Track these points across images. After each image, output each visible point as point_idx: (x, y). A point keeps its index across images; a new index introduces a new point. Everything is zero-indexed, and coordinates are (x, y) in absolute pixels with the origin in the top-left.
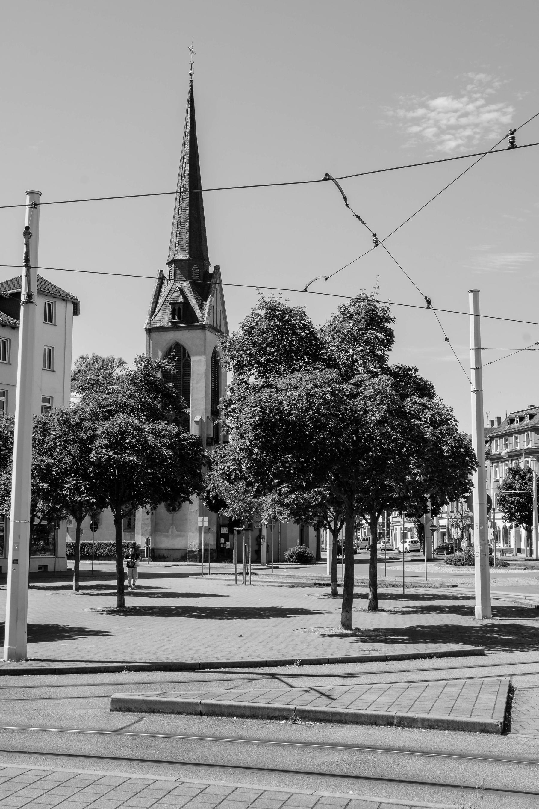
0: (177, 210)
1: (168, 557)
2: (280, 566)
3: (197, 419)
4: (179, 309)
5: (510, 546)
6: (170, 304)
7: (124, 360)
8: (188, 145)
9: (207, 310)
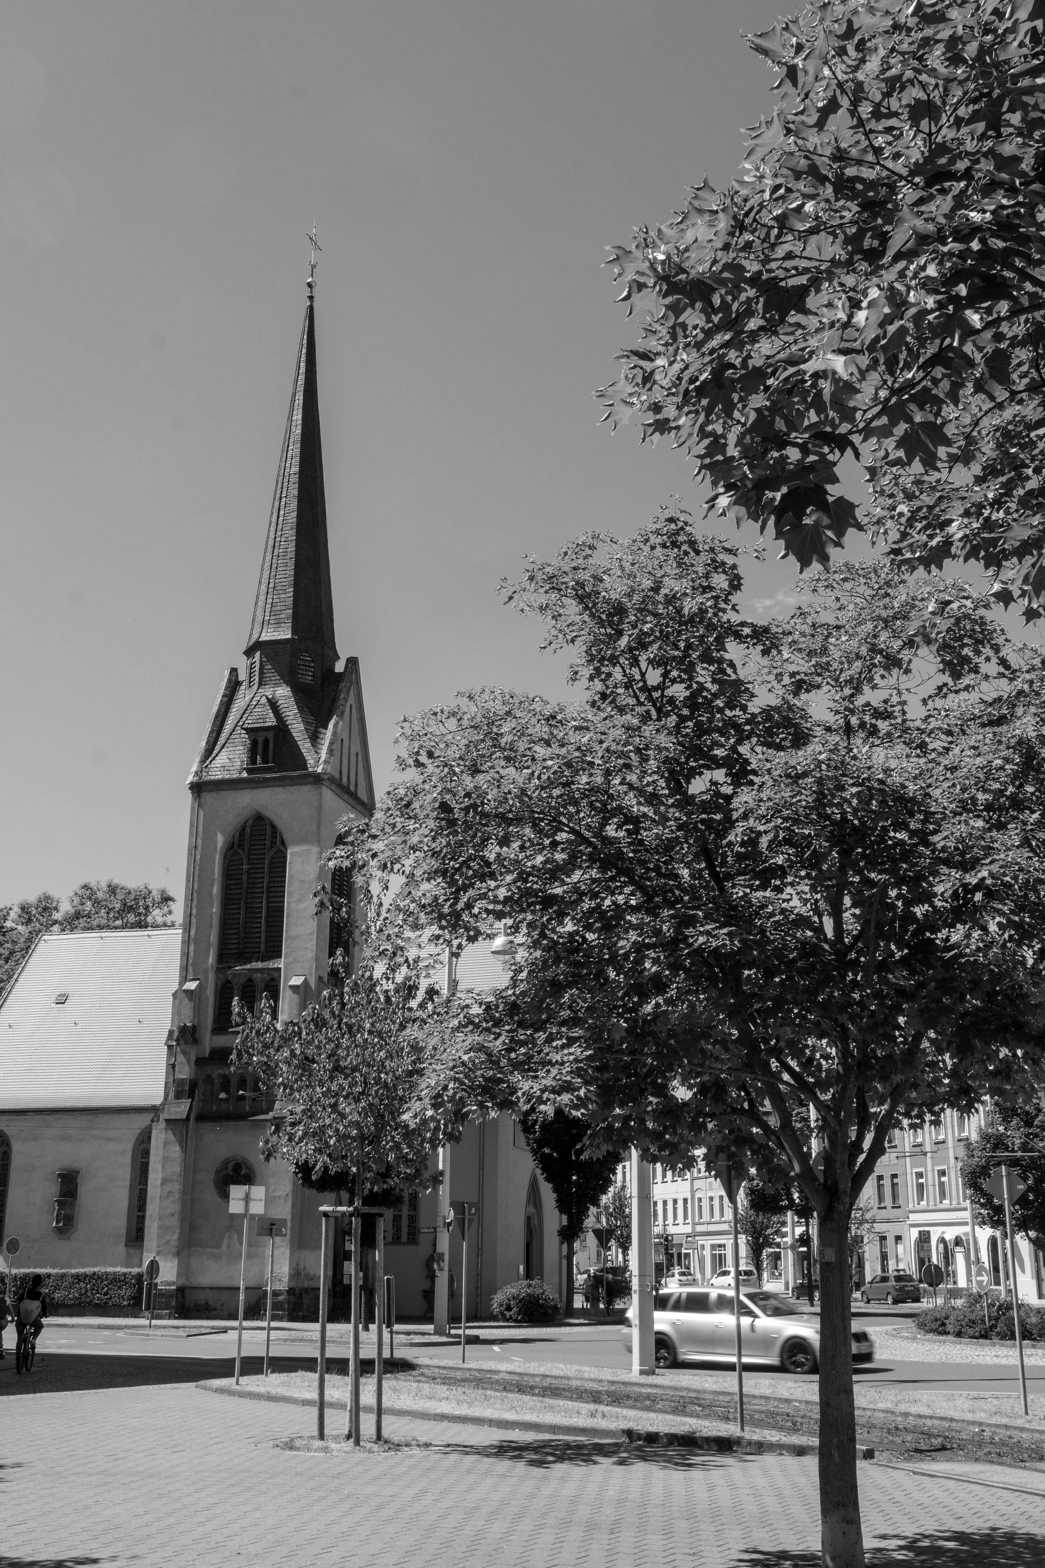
0: (271, 543)
1: (215, 1309)
2: (483, 1333)
3: (296, 981)
4: (266, 742)
5: (955, 1283)
6: (249, 731)
7: (171, 894)
8: (300, 416)
9: (327, 743)
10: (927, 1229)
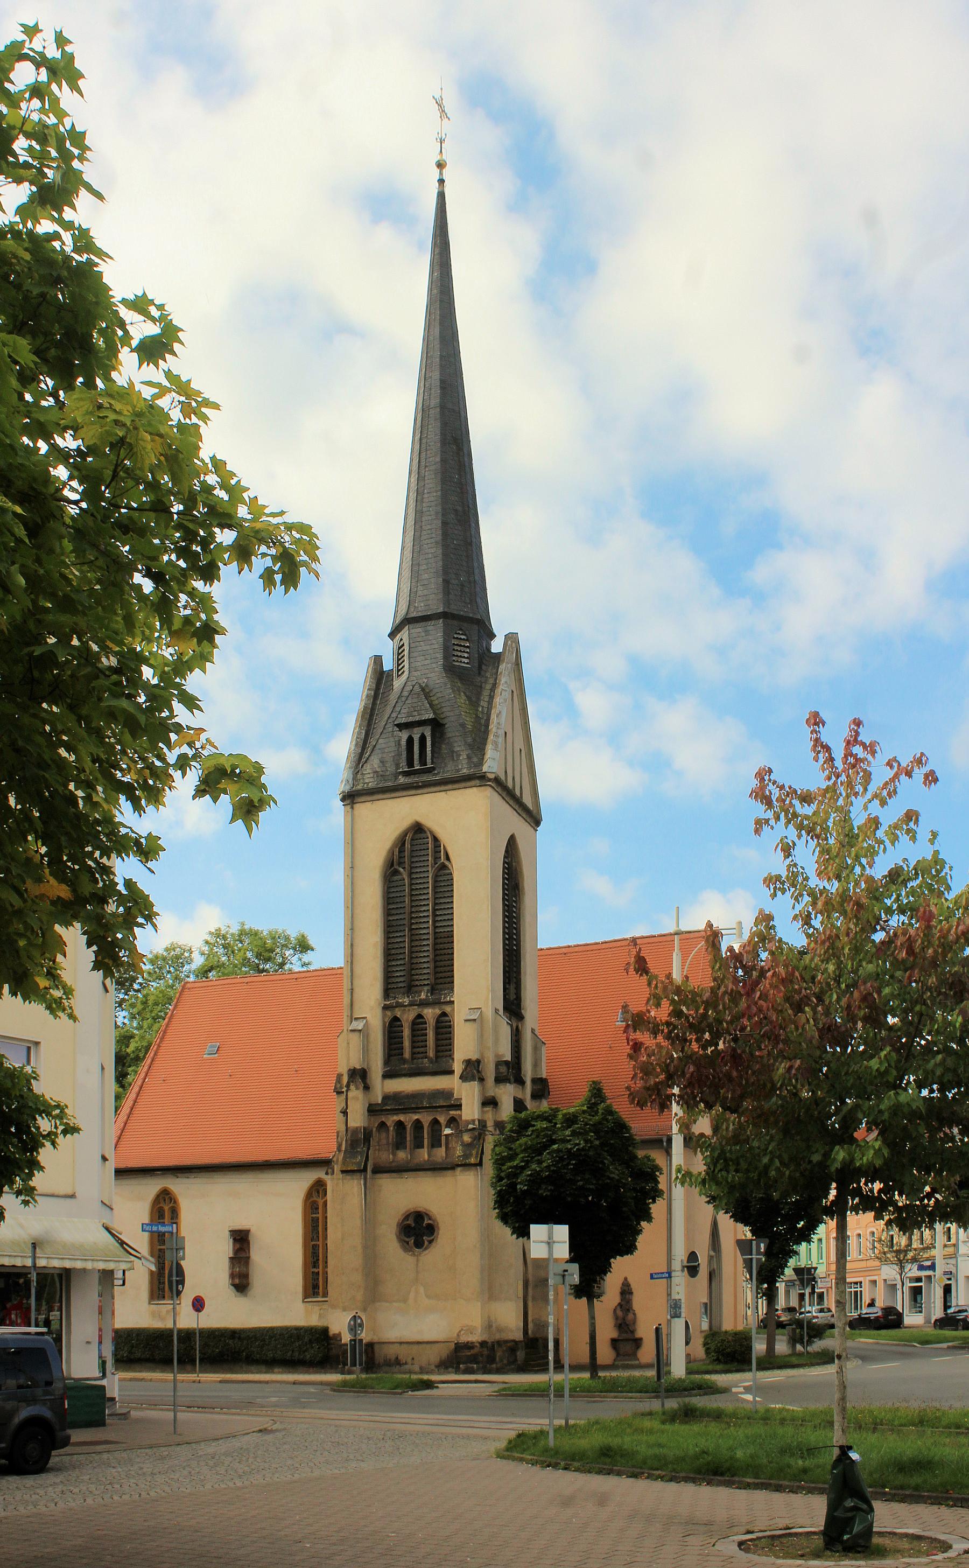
7: (312, 942)
10: (665, 1196)
